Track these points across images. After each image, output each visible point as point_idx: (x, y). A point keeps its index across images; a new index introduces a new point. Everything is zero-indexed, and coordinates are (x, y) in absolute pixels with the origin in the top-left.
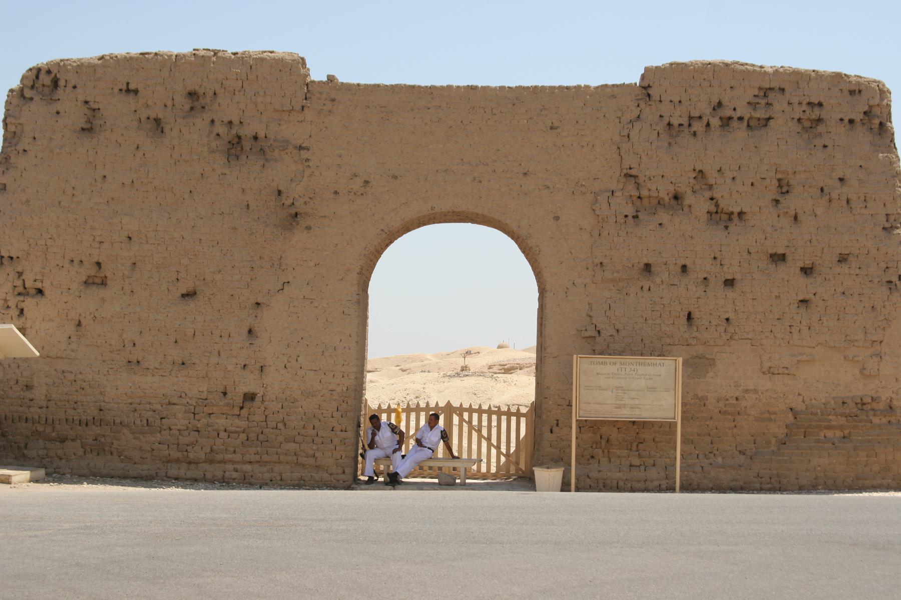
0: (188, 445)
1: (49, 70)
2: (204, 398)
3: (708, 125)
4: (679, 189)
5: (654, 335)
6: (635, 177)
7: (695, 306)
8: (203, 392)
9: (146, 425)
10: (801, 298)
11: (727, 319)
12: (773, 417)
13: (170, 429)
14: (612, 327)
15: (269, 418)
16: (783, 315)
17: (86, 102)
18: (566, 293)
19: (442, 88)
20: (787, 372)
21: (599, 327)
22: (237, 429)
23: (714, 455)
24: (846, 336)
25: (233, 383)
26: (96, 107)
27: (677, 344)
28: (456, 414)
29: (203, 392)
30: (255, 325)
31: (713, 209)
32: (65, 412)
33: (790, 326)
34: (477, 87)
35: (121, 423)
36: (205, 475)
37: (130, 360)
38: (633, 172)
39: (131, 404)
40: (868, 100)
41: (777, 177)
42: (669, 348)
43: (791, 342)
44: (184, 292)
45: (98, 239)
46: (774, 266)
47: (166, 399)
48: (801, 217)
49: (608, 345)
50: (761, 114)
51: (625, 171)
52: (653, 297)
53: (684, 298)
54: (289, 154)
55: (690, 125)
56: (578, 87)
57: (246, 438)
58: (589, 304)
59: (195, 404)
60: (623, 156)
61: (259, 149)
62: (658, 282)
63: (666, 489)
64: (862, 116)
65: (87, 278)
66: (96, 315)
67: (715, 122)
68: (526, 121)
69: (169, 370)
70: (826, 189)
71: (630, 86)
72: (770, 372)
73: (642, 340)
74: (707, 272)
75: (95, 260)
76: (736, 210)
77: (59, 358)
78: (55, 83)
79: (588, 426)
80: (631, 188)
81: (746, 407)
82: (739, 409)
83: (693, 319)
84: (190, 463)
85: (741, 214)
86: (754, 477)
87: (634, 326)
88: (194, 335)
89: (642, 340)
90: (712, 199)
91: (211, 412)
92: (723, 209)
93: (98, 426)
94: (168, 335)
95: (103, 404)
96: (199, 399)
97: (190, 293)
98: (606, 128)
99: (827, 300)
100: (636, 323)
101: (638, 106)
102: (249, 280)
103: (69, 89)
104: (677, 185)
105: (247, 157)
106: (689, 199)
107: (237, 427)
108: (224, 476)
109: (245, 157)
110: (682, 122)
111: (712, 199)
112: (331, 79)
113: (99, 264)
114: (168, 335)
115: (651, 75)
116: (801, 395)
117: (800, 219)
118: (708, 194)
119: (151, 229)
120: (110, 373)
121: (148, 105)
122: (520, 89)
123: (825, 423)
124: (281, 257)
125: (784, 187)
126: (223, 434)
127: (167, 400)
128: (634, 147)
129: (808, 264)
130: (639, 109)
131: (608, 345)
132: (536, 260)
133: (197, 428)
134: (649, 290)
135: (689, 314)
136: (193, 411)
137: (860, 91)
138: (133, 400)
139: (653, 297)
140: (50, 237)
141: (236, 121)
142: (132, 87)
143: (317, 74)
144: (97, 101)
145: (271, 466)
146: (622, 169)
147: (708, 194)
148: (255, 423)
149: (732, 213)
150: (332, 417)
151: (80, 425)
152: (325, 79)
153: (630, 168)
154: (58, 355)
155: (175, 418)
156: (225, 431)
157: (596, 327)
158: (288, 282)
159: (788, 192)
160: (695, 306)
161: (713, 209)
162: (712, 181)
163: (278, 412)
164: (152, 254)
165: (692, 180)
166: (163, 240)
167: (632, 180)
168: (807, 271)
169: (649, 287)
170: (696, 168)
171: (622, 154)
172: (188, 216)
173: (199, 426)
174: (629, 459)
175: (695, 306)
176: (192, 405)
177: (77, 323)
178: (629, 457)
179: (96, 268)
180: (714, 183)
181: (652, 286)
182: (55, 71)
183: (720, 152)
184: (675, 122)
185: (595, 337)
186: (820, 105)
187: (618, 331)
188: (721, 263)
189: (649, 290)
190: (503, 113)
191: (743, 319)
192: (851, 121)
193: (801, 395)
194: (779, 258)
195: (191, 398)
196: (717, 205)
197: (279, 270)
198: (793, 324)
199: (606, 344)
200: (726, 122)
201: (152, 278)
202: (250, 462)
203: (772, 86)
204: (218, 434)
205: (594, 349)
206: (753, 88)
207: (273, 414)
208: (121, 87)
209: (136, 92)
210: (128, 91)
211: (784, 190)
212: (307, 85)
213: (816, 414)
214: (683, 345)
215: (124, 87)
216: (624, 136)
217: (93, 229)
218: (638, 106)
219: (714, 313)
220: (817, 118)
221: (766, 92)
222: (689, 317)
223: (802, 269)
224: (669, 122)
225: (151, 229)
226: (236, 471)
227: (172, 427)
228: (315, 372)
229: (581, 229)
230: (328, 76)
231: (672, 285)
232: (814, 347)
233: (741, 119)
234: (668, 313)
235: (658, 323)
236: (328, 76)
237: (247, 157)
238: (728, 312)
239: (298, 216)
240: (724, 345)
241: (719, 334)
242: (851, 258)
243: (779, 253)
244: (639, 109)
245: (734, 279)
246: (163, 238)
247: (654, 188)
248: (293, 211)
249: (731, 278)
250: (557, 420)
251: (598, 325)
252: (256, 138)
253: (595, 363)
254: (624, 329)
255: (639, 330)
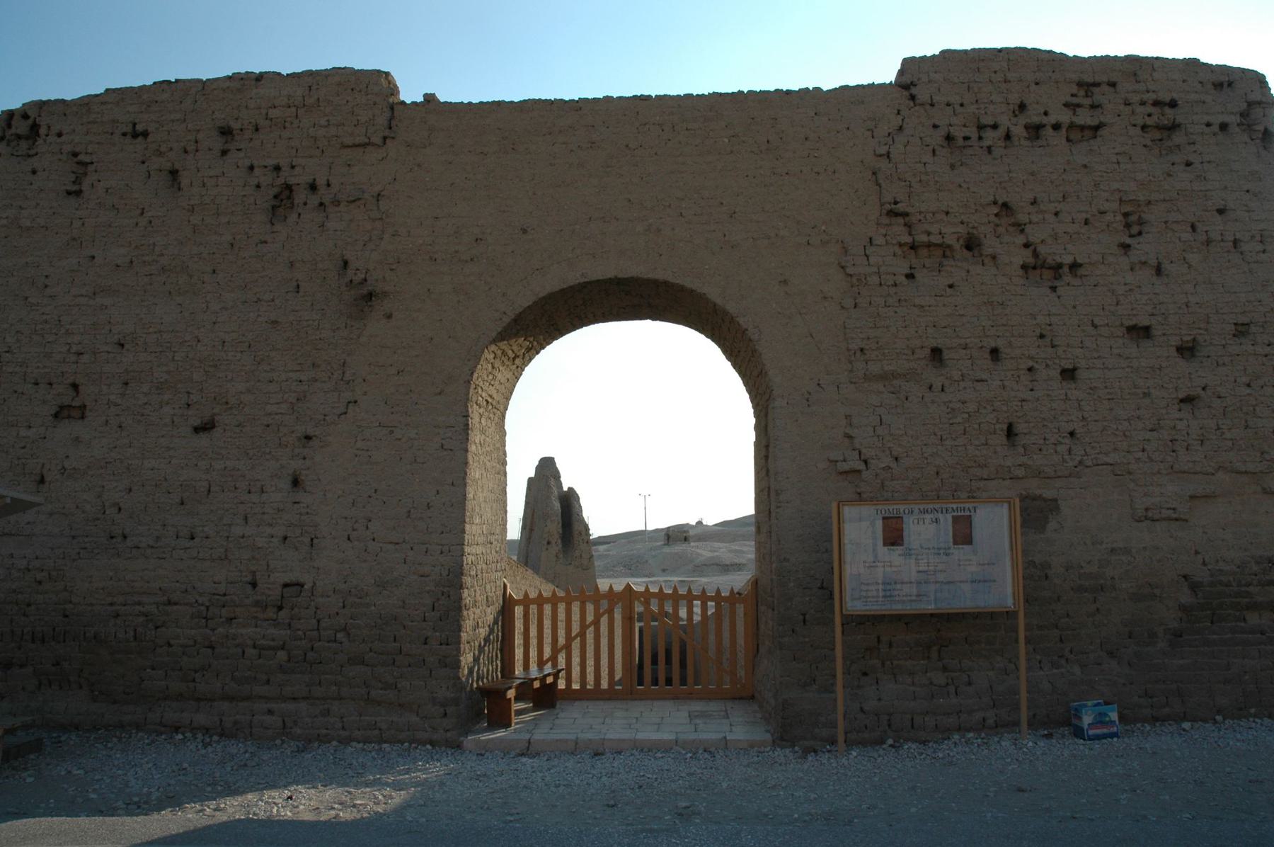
0: (196, 672)
1: (26, 113)
2: (221, 593)
3: (1008, 137)
4: (975, 231)
5: (957, 464)
6: (905, 215)
7: (1018, 414)
8: (220, 583)
9: (132, 639)
10: (1181, 395)
11: (1072, 434)
12: (1157, 592)
13: (170, 645)
14: (888, 452)
15: (323, 624)
16: (1159, 424)
17: (75, 155)
18: (808, 400)
19: (596, 101)
20: (1175, 516)
21: (867, 453)
22: (272, 643)
23: (1067, 660)
24: (1262, 453)
25: (266, 567)
26: (87, 159)
27: (993, 477)
28: (640, 602)
29: (220, 583)
30: (303, 472)
31: (1031, 260)
32: (11, 621)
33: (1171, 441)
34: (649, 97)
35: (95, 637)
36: (221, 721)
37: (112, 535)
38: (900, 207)
39: (111, 604)
40: (1246, 94)
41: (1123, 211)
42: (982, 484)
43: (1176, 466)
44: (197, 422)
45: (74, 349)
46: (1135, 346)
47: (164, 595)
48: (1166, 265)
49: (883, 483)
50: (1084, 118)
51: (888, 207)
52: (950, 402)
53: (1000, 401)
54: (362, 207)
55: (980, 138)
56: (805, 91)
57: (286, 658)
58: (846, 417)
59: (207, 604)
60: (883, 185)
61: (316, 203)
62: (956, 378)
63: (994, 725)
64: (1238, 119)
65: (58, 409)
66: (66, 466)
67: (1018, 131)
68: (726, 140)
69: (170, 549)
70: (1199, 226)
71: (882, 86)
72: (1147, 517)
73: (937, 473)
74: (1032, 358)
75: (70, 380)
76: (1068, 260)
77: (7, 534)
78: (35, 128)
79: (857, 622)
80: (899, 232)
81: (1113, 578)
82: (1102, 581)
83: (1016, 435)
84: (199, 700)
85: (1074, 266)
86: (1139, 697)
87: (924, 450)
88: (209, 491)
89: (937, 473)
90: (1026, 246)
91: (233, 615)
92: (1045, 261)
93: (59, 642)
94: (169, 493)
95: (69, 606)
96: (214, 594)
97: (208, 426)
98: (852, 145)
99: (1226, 397)
100: (925, 445)
101: (898, 113)
102: (294, 401)
103: (52, 139)
104: (970, 225)
105: (300, 214)
106: (990, 244)
107: (273, 640)
108: (251, 721)
109: (295, 216)
110: (968, 134)
111: (1026, 246)
112: (430, 98)
113: (75, 386)
114: (169, 493)
115: (910, 65)
116: (1199, 553)
117: (1166, 273)
118: (1021, 240)
119: (151, 330)
120: (81, 556)
121: (161, 153)
122: (717, 97)
123: (1246, 600)
124: (344, 363)
125: (1133, 224)
126: (250, 652)
127: (166, 598)
128: (899, 171)
129: (1187, 342)
130: (900, 118)
131: (883, 483)
132: (755, 351)
133: (211, 642)
134: (943, 390)
135: (1010, 427)
136: (204, 616)
137: (1230, 84)
138: (115, 599)
139: (950, 402)
140: (6, 349)
141: (284, 163)
142: (139, 128)
143: (410, 93)
144: (89, 151)
145: (326, 706)
146: (882, 205)
147: (1021, 240)
148: (300, 633)
149: (1060, 266)
150: (425, 621)
151: (33, 641)
152: (420, 99)
153: (896, 203)
154: (13, 532)
155: (177, 627)
156: (255, 647)
157: (860, 454)
158: (356, 402)
159: (1140, 233)
160: (1019, 414)
161: (1031, 260)
162: (1022, 218)
163: (337, 614)
164: (151, 368)
165: (993, 218)
166: (168, 345)
167: (900, 220)
168: (1187, 350)
169: (943, 386)
170: (997, 197)
171: (881, 181)
172: (207, 307)
173: (213, 638)
174: (928, 674)
175: (1018, 414)
176: (202, 605)
177: (38, 478)
178: (926, 672)
179: (71, 392)
180: (1028, 221)
181: (947, 383)
182: (32, 114)
183: (1032, 174)
184: (958, 133)
185: (859, 471)
186: (1173, 104)
187: (896, 459)
188: (1052, 344)
189: (943, 390)
190: (691, 130)
191: (1097, 431)
192: (1224, 127)
193: (1199, 553)
194: (1141, 332)
195: (201, 595)
196: (1036, 254)
197: (342, 383)
198: (1176, 437)
199: (879, 481)
200: (1035, 131)
201: (150, 404)
202: (294, 699)
203: (1098, 79)
204: (244, 652)
205: (859, 490)
206: (1070, 83)
207: (330, 617)
208: (125, 130)
209: (145, 134)
210: (135, 135)
211: (1135, 230)
212: (392, 108)
213: (1228, 585)
214: (1004, 479)
215: (129, 129)
216: (881, 156)
217: (68, 333)
218: (898, 113)
219: (1049, 425)
220: (1170, 125)
221: (1087, 87)
222: (1010, 432)
223: (1180, 349)
224: (948, 135)
225: (151, 330)
226: (270, 712)
227: (172, 642)
228: (397, 546)
229: (825, 298)
230: (426, 96)
231: (977, 381)
232: (1213, 474)
233: (1056, 127)
234: (976, 426)
235: (962, 443)
236: (426, 96)
237: (300, 214)
238: (1072, 421)
239: (373, 299)
240: (1070, 476)
241: (1060, 456)
242: (1253, 329)
243: (1141, 325)
244: (900, 118)
245: (1075, 369)
246: (169, 342)
247: (934, 229)
248: (365, 291)
249: (1071, 367)
250: (804, 615)
251: (864, 451)
252: (313, 187)
253: (929, 510)
254: (907, 456)
255: (931, 455)
